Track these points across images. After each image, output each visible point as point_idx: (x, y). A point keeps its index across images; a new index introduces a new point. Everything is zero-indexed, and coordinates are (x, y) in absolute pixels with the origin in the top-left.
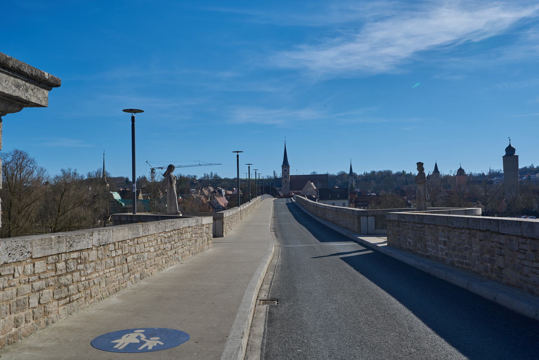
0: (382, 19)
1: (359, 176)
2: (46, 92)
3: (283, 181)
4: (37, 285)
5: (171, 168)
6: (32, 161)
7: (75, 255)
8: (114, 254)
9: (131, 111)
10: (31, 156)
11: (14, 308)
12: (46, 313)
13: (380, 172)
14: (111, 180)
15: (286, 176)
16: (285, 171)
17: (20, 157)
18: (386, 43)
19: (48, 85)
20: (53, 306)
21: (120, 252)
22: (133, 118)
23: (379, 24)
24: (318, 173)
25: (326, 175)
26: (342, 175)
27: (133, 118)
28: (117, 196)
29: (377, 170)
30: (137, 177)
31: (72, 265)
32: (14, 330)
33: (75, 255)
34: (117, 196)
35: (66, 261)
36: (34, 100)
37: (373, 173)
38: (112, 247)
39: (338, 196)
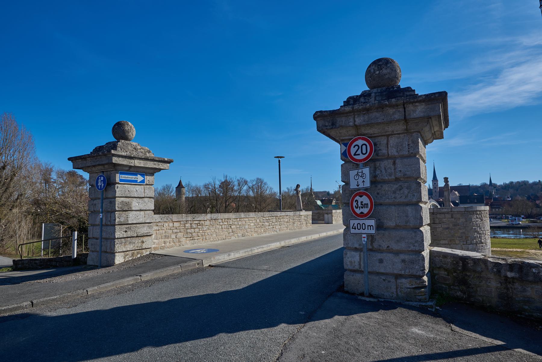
0: (518, 64)
1: (499, 186)
2: (168, 165)
3: (434, 191)
4: (175, 231)
5: (298, 186)
6: (265, 184)
7: (196, 222)
8: (221, 224)
9: (278, 157)
10: (265, 181)
11: (164, 237)
12: (179, 241)
13: (518, 182)
14: (317, 194)
15: (435, 188)
16: (435, 184)
17: (260, 181)
18: (523, 82)
19: (169, 162)
20: (183, 240)
21: (226, 223)
22: (279, 161)
23: (515, 69)
24: (464, 184)
25: (469, 186)
26: (484, 186)
27: (279, 161)
28: (319, 203)
29: (515, 180)
30: (282, 192)
31: (194, 226)
32: (163, 245)
33: (196, 222)
34: (319, 203)
35: (191, 224)
36: (162, 168)
37: (512, 183)
38: (220, 221)
39: (476, 201)
